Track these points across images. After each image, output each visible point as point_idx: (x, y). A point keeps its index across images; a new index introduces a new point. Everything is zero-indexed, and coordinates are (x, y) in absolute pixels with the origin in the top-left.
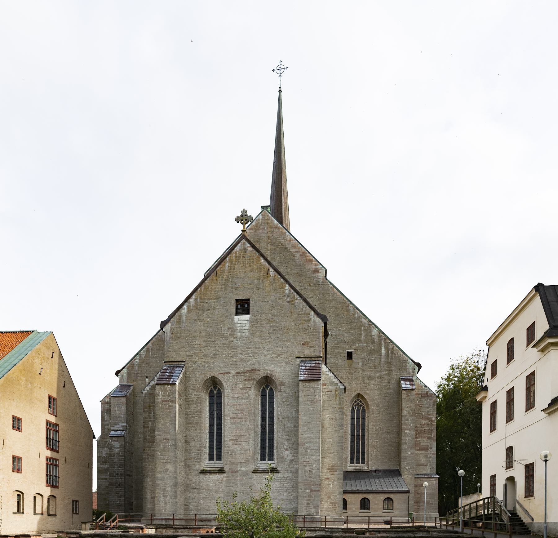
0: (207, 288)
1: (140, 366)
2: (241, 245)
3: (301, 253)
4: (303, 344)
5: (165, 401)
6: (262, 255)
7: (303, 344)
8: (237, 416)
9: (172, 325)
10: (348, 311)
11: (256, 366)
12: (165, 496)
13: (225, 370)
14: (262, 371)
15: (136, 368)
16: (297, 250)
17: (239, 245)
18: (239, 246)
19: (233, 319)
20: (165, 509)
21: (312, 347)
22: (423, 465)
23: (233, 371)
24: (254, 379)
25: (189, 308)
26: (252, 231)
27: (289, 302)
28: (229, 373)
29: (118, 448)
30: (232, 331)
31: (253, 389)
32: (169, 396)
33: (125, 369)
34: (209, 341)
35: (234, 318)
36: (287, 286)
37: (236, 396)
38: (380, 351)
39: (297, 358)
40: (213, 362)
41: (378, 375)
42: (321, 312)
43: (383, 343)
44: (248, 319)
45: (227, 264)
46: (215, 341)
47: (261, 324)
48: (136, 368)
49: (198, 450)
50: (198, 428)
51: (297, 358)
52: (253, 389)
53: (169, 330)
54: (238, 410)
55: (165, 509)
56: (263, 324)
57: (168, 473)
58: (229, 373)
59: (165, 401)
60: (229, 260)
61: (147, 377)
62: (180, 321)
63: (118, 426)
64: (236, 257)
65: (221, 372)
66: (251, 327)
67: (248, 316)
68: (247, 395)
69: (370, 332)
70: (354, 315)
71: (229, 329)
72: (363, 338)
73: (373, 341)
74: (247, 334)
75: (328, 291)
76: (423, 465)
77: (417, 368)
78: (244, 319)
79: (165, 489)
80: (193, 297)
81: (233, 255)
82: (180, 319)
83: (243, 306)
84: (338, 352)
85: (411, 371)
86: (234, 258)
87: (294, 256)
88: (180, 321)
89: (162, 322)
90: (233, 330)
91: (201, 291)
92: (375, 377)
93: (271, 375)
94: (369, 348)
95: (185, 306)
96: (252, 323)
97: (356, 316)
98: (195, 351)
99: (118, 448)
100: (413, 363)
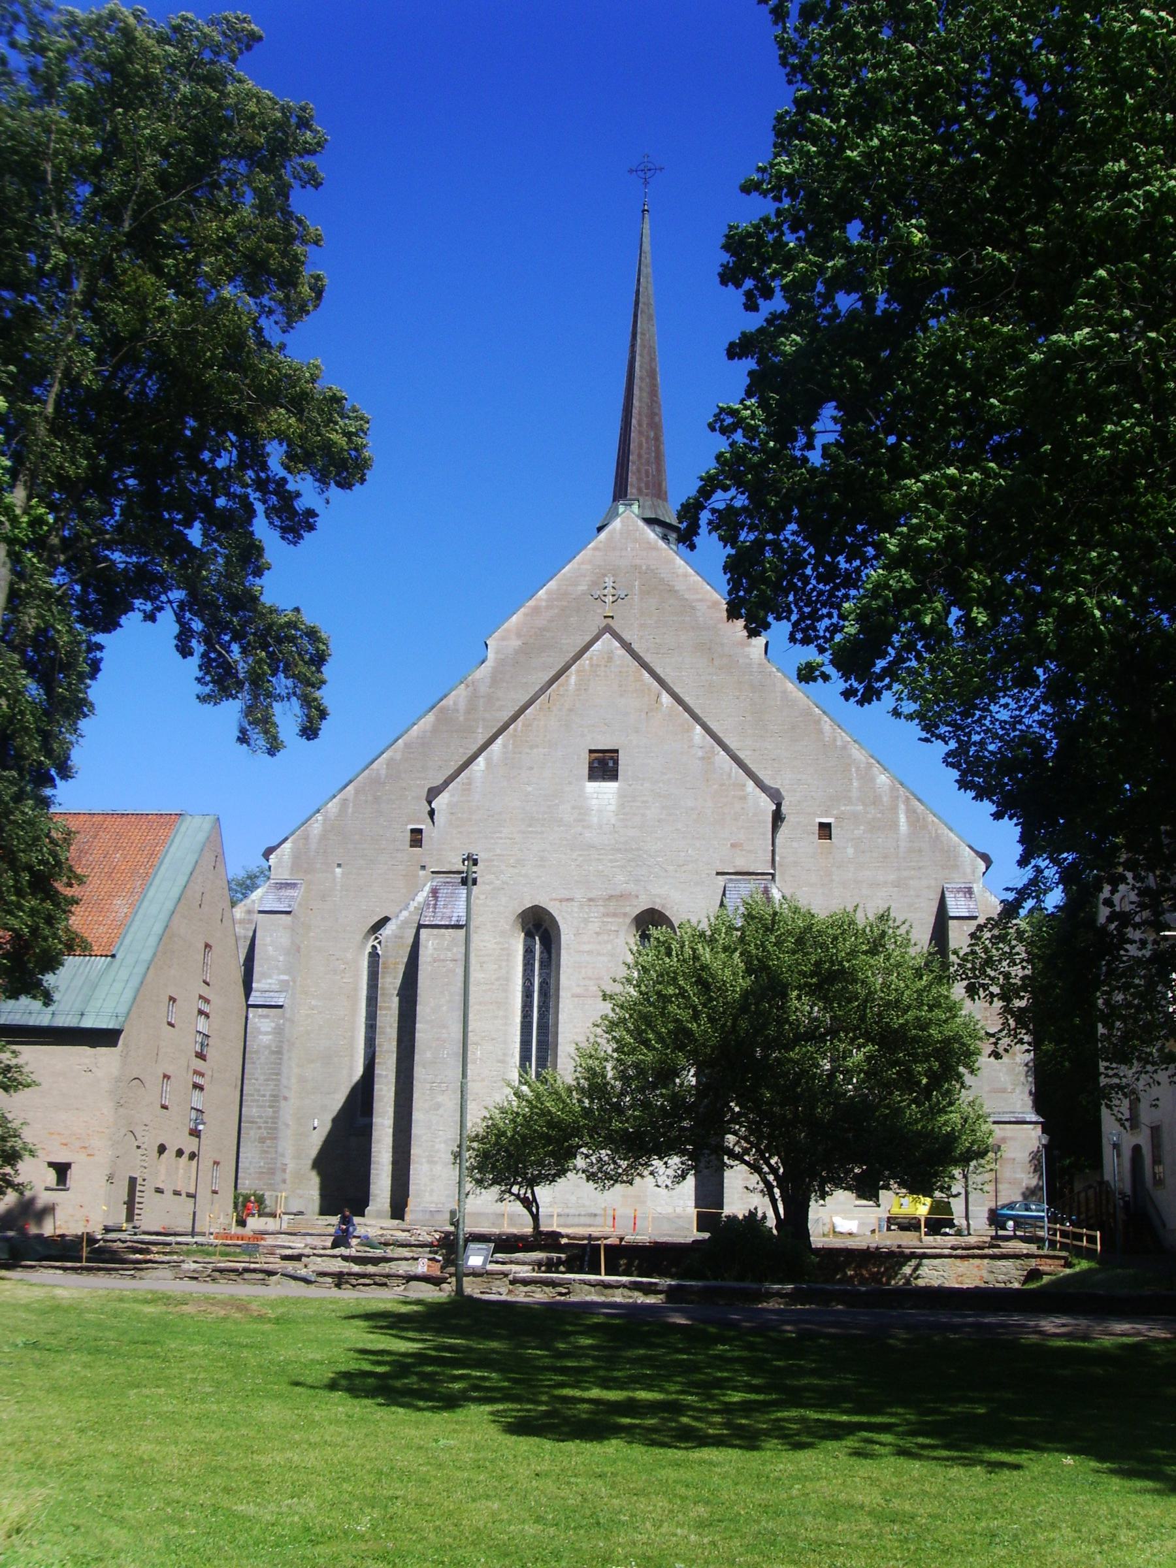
0: (527, 725)
1: (324, 837)
2: (603, 643)
3: (709, 604)
4: (733, 845)
5: (439, 960)
6: (645, 665)
7: (733, 845)
8: (587, 990)
9: (452, 795)
10: (821, 732)
11: (631, 887)
12: (431, 1162)
13: (566, 894)
14: (643, 898)
15: (313, 845)
16: (699, 597)
17: (599, 643)
18: (597, 646)
19: (582, 789)
20: (432, 1190)
21: (750, 851)
22: (1004, 1091)
23: (579, 894)
24: (625, 914)
25: (488, 761)
26: (597, 553)
27: (702, 758)
28: (572, 900)
29: (267, 1033)
30: (580, 814)
31: (622, 934)
32: (449, 950)
33: (287, 846)
34: (531, 832)
35: (584, 787)
36: (698, 727)
37: (586, 948)
38: (895, 825)
39: (718, 874)
40: (539, 877)
41: (892, 877)
42: (768, 782)
43: (902, 807)
44: (615, 790)
45: (573, 679)
46: (542, 833)
47: (643, 802)
48: (313, 845)
49: (499, 1061)
50: (501, 1013)
51: (718, 874)
52: (622, 934)
53: (444, 807)
54: (590, 979)
55: (432, 1190)
56: (646, 802)
57: (441, 1111)
58: (572, 900)
59: (439, 960)
60: (578, 671)
61: (339, 865)
62: (469, 790)
63: (270, 981)
64: (591, 665)
65: (554, 896)
66: (621, 806)
67: (611, 786)
68: (609, 947)
69: (873, 779)
70: (835, 740)
71: (573, 808)
72: (855, 794)
73: (876, 801)
74: (613, 821)
75: (774, 685)
76: (1004, 1091)
77: (982, 866)
78: (606, 790)
79: (433, 1146)
80: (499, 741)
81: (585, 661)
82: (470, 784)
83: (604, 766)
84: (798, 823)
85: (969, 870)
86: (587, 668)
87: (693, 608)
88: (468, 787)
89: (430, 790)
90: (582, 811)
91: (515, 730)
92: (886, 883)
93: (899, 1246)
94: (870, 816)
95: (480, 759)
96: (621, 795)
97: (839, 743)
98: (498, 851)
99: (267, 1033)
100: (972, 853)
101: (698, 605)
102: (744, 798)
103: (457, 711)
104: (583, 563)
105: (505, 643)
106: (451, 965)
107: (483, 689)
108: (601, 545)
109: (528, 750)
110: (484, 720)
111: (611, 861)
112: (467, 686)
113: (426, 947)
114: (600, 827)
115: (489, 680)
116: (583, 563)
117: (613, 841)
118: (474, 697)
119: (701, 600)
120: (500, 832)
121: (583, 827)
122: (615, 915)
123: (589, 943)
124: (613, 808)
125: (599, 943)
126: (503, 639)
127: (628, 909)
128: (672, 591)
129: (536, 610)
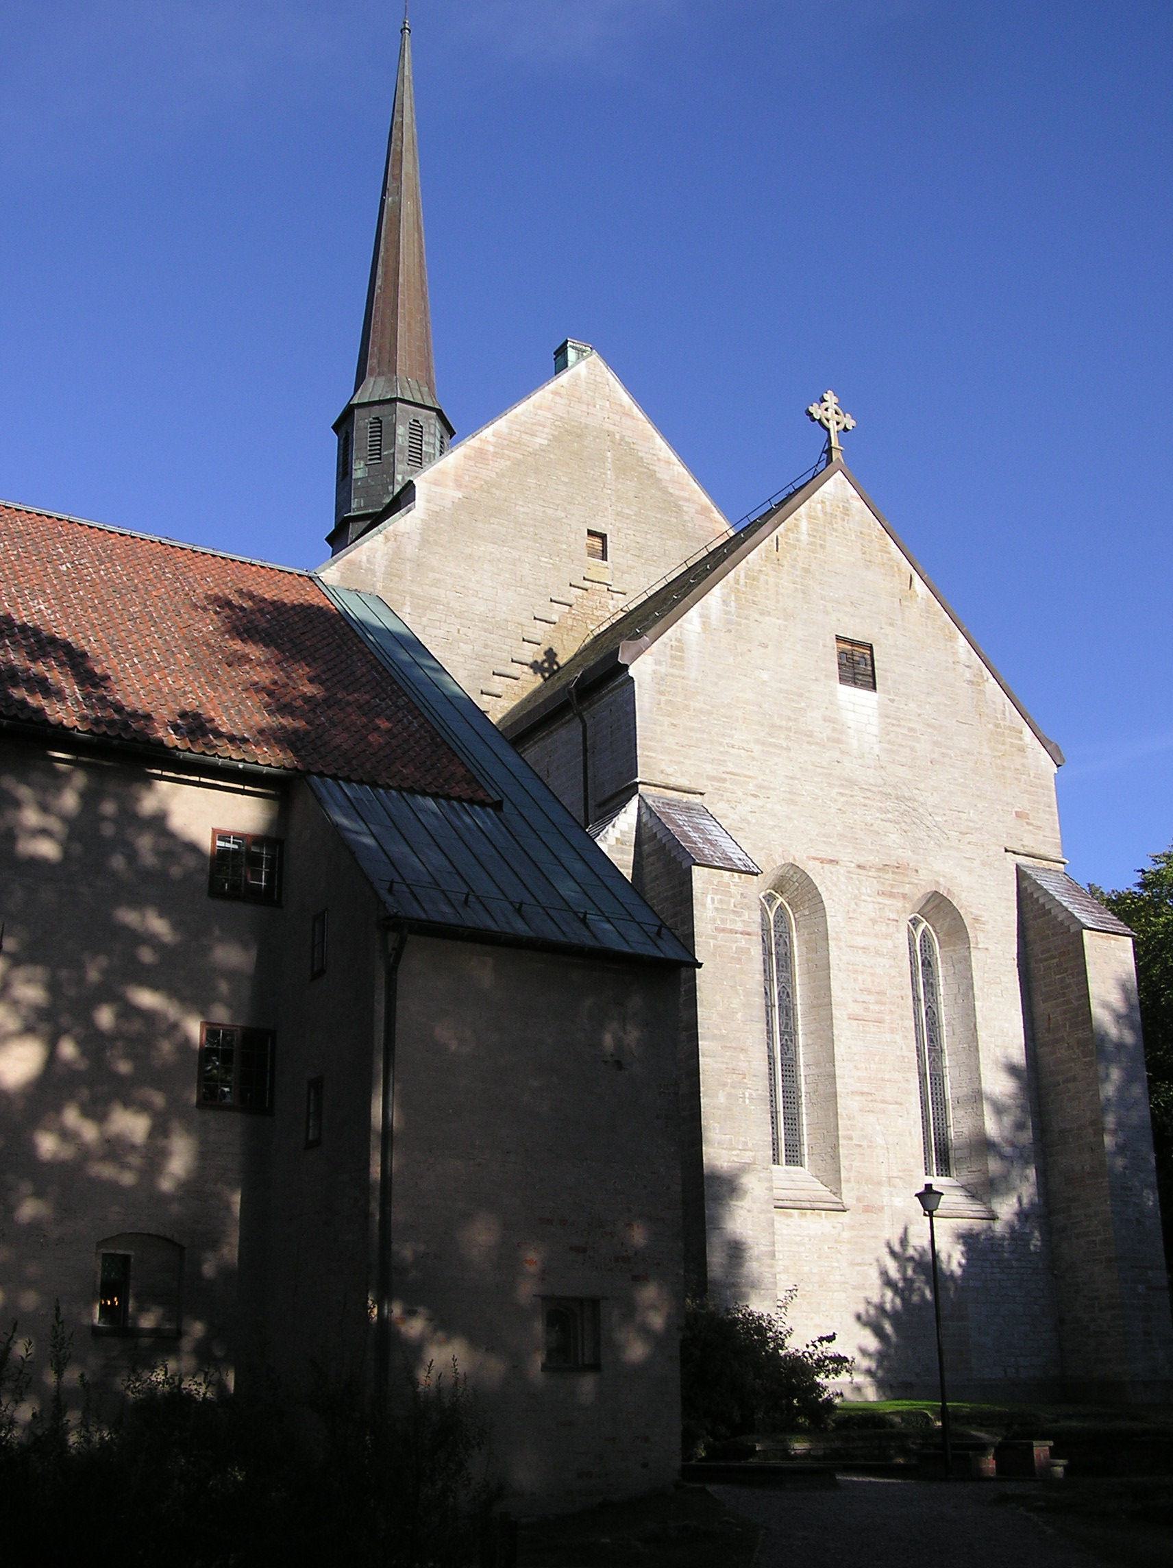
4: (1018, 815)
13: (828, 853)
16: (686, 495)
24: (904, 896)
27: (971, 682)
34: (771, 744)
37: (860, 941)
47: (910, 729)
54: (870, 993)
68: (890, 943)
74: (876, 751)
83: (857, 665)
98: (731, 767)
101: (686, 507)
102: (1022, 750)
103: (373, 572)
104: (540, 408)
105: (438, 489)
106: (743, 942)
107: (410, 550)
108: (563, 391)
109: (757, 616)
110: (412, 594)
111: (880, 810)
112: (387, 539)
113: (704, 905)
114: (862, 757)
115: (418, 538)
116: (540, 408)
117: (880, 781)
118: (396, 557)
119: (687, 500)
120: (731, 736)
121: (842, 752)
122: (892, 895)
123: (864, 934)
124: (874, 730)
125: (876, 936)
126: (436, 483)
127: (907, 889)
128: (652, 475)
129: (481, 455)
